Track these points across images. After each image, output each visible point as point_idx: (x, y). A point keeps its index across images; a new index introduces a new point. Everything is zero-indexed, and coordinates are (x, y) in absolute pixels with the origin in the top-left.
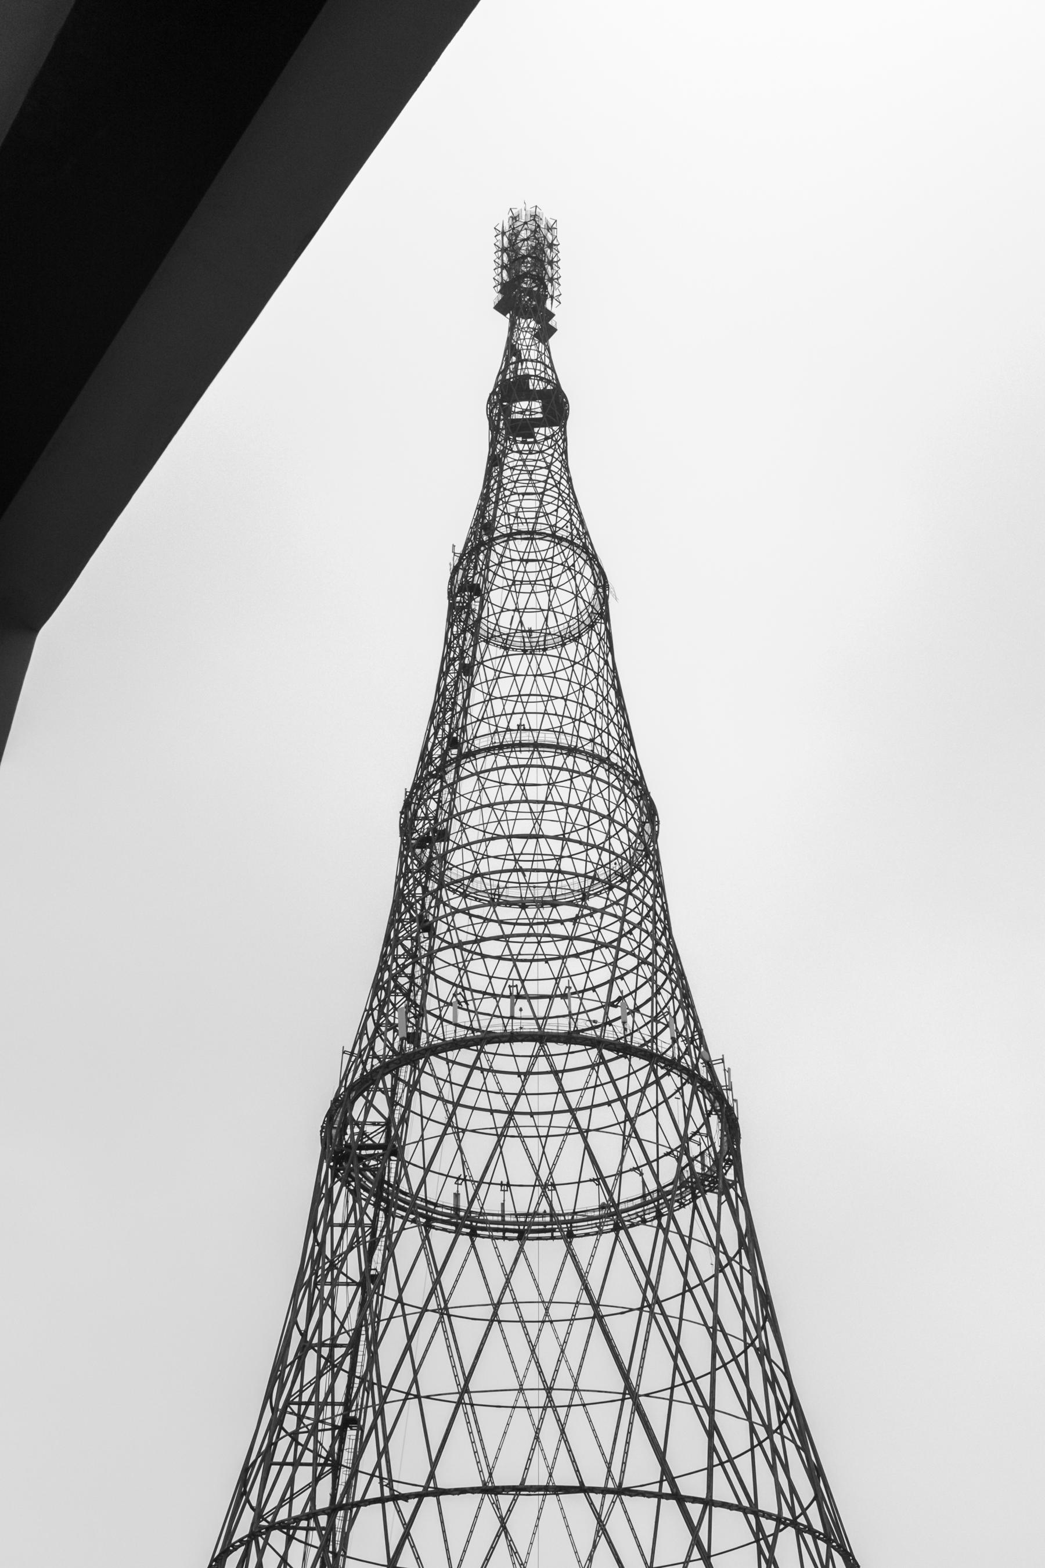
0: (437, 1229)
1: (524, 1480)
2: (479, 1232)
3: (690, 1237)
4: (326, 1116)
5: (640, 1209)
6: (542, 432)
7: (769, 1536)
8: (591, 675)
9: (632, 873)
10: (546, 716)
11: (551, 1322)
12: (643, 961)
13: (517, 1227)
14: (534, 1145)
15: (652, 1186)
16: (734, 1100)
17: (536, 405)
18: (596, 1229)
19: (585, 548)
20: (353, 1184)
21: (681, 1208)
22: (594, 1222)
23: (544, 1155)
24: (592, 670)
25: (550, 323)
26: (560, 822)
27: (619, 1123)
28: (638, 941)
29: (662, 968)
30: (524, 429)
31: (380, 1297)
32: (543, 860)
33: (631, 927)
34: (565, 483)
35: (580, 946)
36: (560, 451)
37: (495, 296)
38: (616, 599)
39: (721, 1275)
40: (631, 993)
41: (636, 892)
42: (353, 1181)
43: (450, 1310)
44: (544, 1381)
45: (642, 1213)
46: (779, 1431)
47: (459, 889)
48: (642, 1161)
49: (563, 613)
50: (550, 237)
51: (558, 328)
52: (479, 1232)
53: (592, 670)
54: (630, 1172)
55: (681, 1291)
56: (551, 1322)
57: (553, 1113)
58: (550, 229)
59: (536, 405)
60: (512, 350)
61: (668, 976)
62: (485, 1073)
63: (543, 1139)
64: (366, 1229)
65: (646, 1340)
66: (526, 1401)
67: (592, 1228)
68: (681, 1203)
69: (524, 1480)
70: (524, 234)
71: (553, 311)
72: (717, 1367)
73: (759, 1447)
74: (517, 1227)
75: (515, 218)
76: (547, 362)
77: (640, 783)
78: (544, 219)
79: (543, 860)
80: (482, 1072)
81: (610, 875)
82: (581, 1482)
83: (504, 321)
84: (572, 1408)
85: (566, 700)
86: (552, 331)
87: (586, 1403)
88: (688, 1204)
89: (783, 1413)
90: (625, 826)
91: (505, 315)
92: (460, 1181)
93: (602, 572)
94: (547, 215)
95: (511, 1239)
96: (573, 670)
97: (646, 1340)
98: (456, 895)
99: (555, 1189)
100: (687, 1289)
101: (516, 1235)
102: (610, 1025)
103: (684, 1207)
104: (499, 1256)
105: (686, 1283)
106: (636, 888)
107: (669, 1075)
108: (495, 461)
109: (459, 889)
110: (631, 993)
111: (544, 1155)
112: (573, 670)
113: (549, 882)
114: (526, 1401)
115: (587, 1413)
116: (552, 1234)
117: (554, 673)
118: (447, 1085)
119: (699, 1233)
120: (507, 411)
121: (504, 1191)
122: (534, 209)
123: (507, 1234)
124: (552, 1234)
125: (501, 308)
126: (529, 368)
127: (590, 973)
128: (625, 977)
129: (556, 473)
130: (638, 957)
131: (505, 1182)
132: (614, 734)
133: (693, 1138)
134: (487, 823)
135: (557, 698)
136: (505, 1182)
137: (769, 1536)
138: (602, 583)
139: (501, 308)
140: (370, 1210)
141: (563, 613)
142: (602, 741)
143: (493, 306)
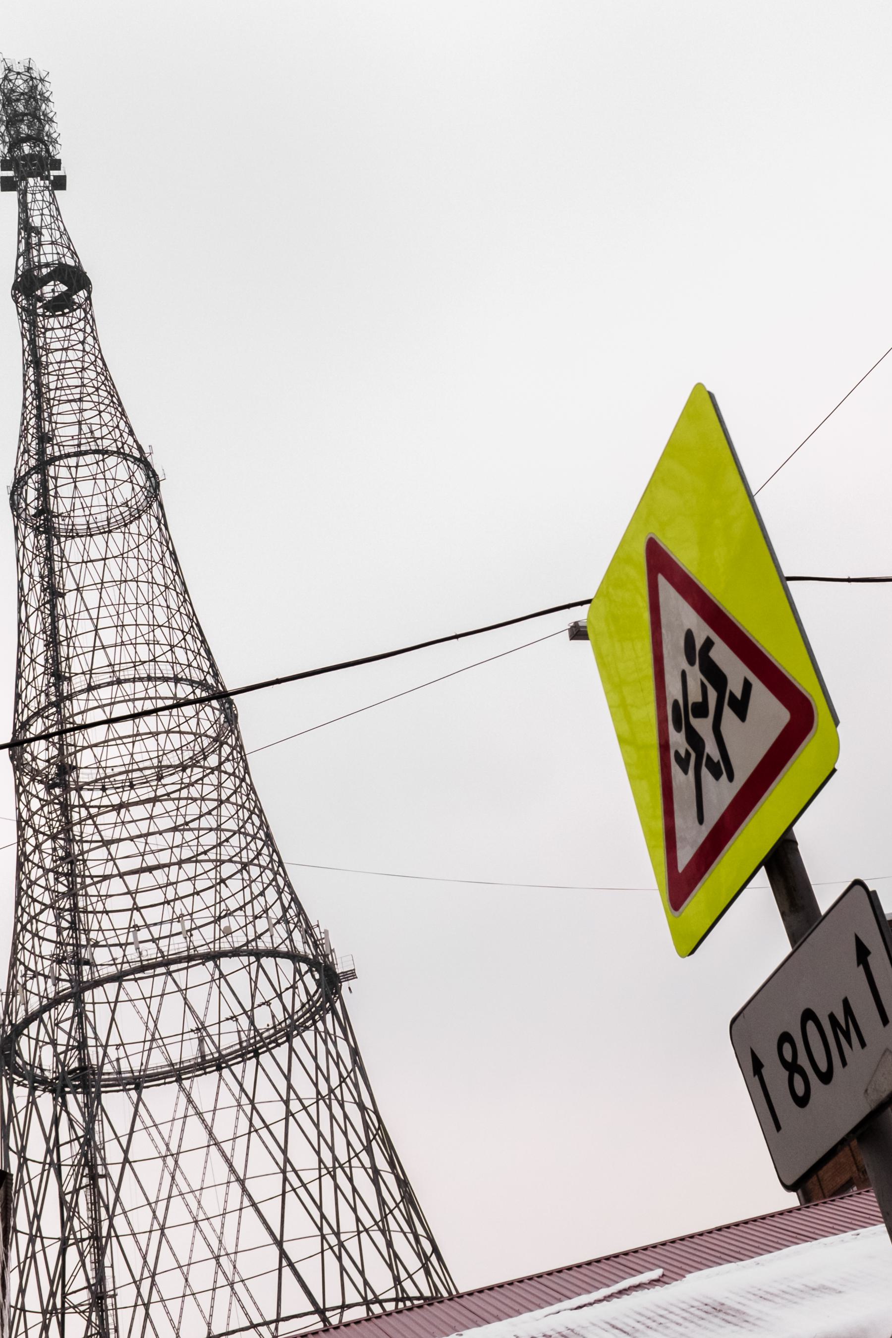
8: (195, 664)
14: (141, 1005)
15: (280, 1017)
24: (138, 485)
26: (109, 1003)
27: (245, 967)
32: (142, 740)
39: (343, 1084)
40: (256, 897)
44: (212, 1252)
48: (238, 1010)
49: (160, 605)
53: (138, 485)
63: (148, 1000)
66: (205, 1214)
73: (390, 1215)
79: (142, 740)
80: (121, 947)
82: (251, 1322)
85: (137, 582)
89: (379, 1136)
96: (139, 551)
100: (320, 1097)
102: (260, 939)
105: (318, 1093)
110: (256, 897)
112: (139, 551)
113: (178, 809)
114: (205, 1214)
117: (122, 555)
118: (40, 959)
119: (347, 1097)
122: (27, 61)
127: (200, 839)
135: (131, 581)
141: (160, 605)
142: (246, 838)
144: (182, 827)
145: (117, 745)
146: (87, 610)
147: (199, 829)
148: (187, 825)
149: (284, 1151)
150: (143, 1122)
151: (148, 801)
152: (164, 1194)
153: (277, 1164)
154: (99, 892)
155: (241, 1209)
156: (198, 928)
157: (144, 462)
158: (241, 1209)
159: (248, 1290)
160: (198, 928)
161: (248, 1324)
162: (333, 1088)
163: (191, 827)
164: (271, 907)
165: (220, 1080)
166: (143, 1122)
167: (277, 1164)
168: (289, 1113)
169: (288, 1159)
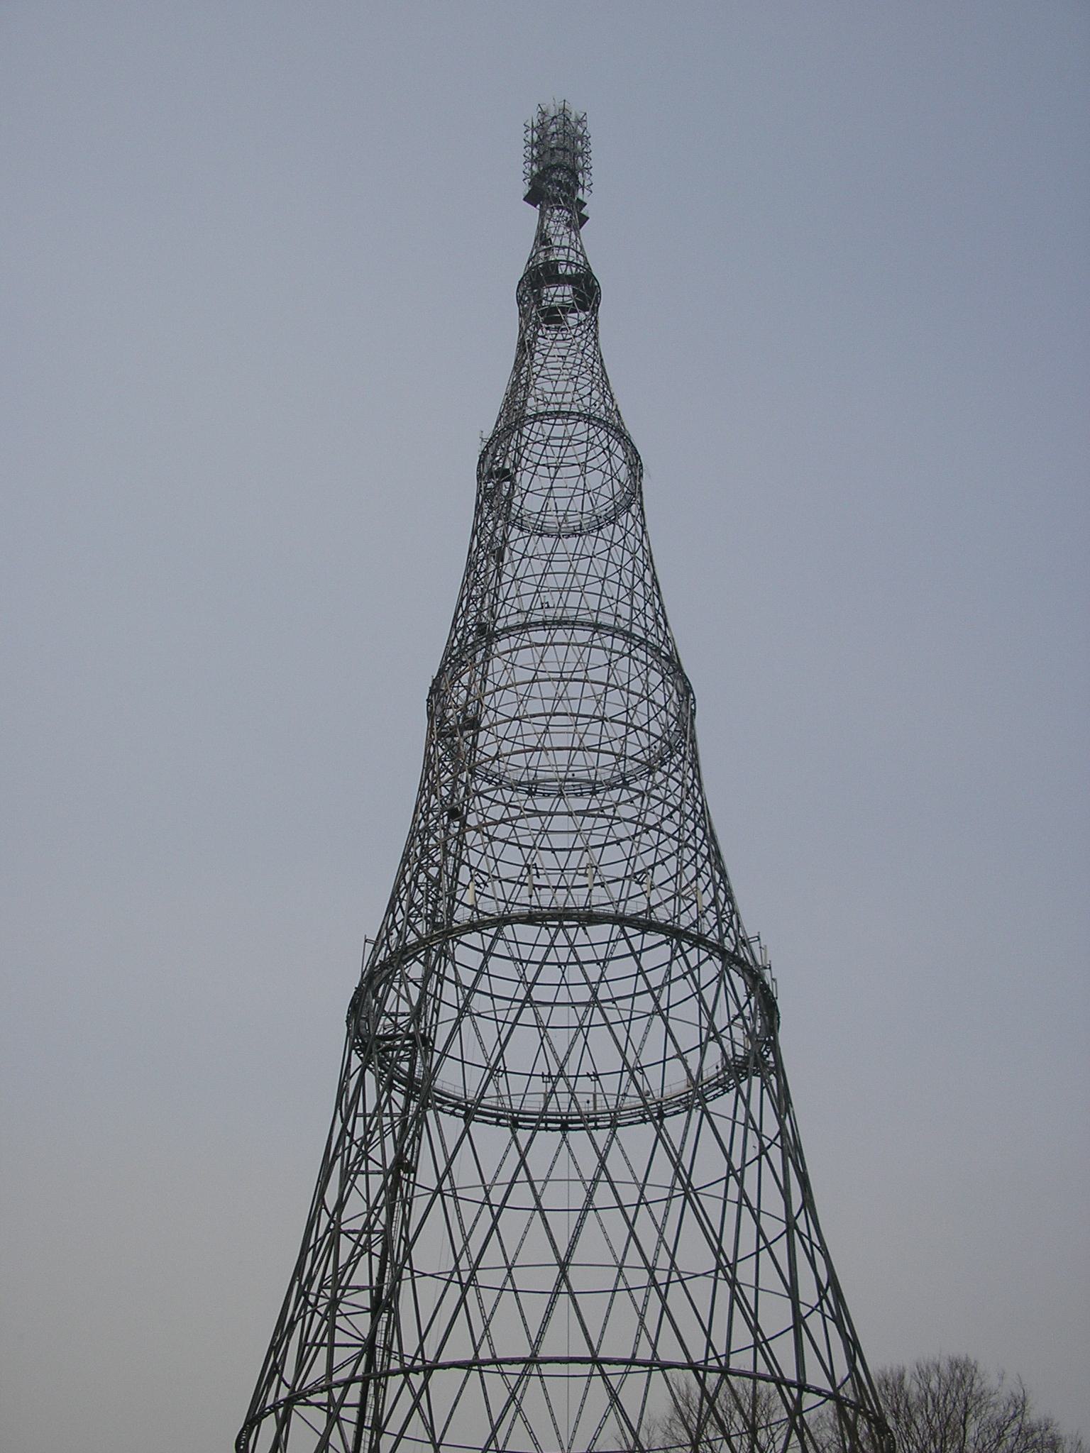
0: (477, 1121)
1: (634, 1355)
2: (520, 1123)
3: (759, 1211)
4: (350, 1006)
5: (684, 1096)
6: (572, 319)
7: (764, 1248)
9: (671, 756)
10: (497, 857)
11: (595, 1210)
12: (649, 696)
13: (559, 1118)
16: (773, 979)
17: (568, 290)
18: (640, 1118)
19: (618, 430)
20: (386, 1075)
21: (725, 1093)
22: (637, 1110)
23: (586, 1046)
25: (582, 212)
28: (678, 823)
29: (704, 869)
30: (553, 317)
31: (411, 1185)
33: (672, 809)
34: (598, 366)
35: (621, 830)
36: (592, 335)
37: (525, 189)
38: (650, 476)
41: (675, 775)
42: (386, 1073)
43: (457, 1191)
44: (558, 1257)
45: (686, 1100)
46: (819, 1308)
47: (495, 780)
50: (580, 130)
51: (589, 216)
52: (520, 1123)
54: (673, 1060)
55: (725, 1175)
56: (595, 1210)
57: (609, 1025)
58: (579, 122)
59: (568, 290)
60: (543, 239)
61: (708, 858)
62: (524, 964)
64: (395, 1119)
65: (685, 1134)
67: (636, 1116)
68: (725, 1088)
69: (634, 1355)
70: (553, 128)
71: (585, 200)
72: (792, 1330)
74: (559, 1118)
75: (543, 113)
76: (579, 249)
77: (679, 669)
78: (573, 113)
81: (650, 758)
82: (494, 1356)
83: (534, 212)
84: (617, 1293)
86: (584, 219)
87: (631, 1287)
88: (732, 1089)
90: (664, 708)
91: (535, 206)
92: (500, 1073)
93: (635, 452)
94: (575, 111)
95: (553, 1130)
97: (685, 1134)
98: (491, 786)
99: (598, 1079)
101: (559, 1125)
103: (728, 1092)
104: (557, 1155)
106: (676, 770)
107: (711, 959)
108: (525, 348)
109: (495, 780)
111: (586, 1046)
115: (632, 1297)
116: (596, 1124)
120: (538, 299)
121: (546, 1082)
123: (550, 1125)
124: (596, 1124)
125: (531, 198)
126: (561, 255)
128: (666, 862)
129: (590, 357)
130: (679, 840)
131: (546, 1074)
132: (672, 710)
133: (736, 1021)
134: (630, 1021)
136: (546, 1074)
137: (764, 1248)
138: (635, 464)
139: (531, 198)
140: (399, 1098)
143: (523, 197)
144: (596, 812)
145: (515, 1023)
146: (621, 1207)
147: (613, 818)
148: (602, 811)
149: (450, 1162)
150: (497, 1089)
151: (578, 813)
152: (506, 1176)
153: (555, 1248)
154: (514, 829)
155: (614, 1291)
156: (545, 715)
157: (673, 667)
158: (614, 1291)
159: (523, 1317)
160: (545, 715)
161: (490, 1357)
162: (386, 1430)
163: (607, 813)
164: (671, 878)
165: (618, 1276)
166: (497, 1089)
167: (555, 1248)
168: (588, 1207)
169: (706, 1335)
